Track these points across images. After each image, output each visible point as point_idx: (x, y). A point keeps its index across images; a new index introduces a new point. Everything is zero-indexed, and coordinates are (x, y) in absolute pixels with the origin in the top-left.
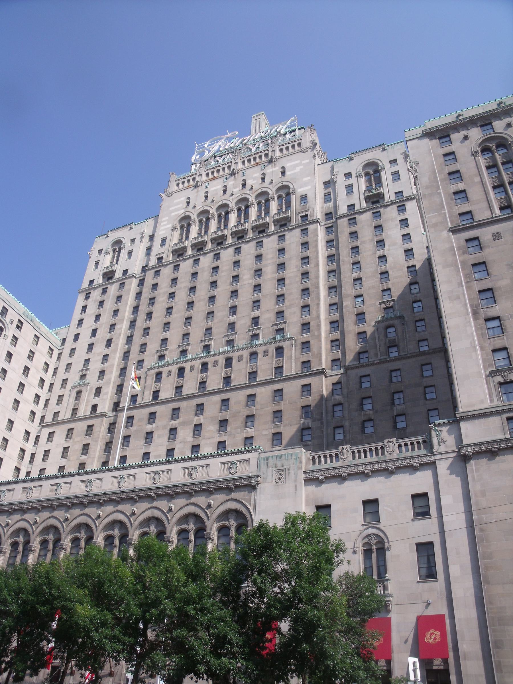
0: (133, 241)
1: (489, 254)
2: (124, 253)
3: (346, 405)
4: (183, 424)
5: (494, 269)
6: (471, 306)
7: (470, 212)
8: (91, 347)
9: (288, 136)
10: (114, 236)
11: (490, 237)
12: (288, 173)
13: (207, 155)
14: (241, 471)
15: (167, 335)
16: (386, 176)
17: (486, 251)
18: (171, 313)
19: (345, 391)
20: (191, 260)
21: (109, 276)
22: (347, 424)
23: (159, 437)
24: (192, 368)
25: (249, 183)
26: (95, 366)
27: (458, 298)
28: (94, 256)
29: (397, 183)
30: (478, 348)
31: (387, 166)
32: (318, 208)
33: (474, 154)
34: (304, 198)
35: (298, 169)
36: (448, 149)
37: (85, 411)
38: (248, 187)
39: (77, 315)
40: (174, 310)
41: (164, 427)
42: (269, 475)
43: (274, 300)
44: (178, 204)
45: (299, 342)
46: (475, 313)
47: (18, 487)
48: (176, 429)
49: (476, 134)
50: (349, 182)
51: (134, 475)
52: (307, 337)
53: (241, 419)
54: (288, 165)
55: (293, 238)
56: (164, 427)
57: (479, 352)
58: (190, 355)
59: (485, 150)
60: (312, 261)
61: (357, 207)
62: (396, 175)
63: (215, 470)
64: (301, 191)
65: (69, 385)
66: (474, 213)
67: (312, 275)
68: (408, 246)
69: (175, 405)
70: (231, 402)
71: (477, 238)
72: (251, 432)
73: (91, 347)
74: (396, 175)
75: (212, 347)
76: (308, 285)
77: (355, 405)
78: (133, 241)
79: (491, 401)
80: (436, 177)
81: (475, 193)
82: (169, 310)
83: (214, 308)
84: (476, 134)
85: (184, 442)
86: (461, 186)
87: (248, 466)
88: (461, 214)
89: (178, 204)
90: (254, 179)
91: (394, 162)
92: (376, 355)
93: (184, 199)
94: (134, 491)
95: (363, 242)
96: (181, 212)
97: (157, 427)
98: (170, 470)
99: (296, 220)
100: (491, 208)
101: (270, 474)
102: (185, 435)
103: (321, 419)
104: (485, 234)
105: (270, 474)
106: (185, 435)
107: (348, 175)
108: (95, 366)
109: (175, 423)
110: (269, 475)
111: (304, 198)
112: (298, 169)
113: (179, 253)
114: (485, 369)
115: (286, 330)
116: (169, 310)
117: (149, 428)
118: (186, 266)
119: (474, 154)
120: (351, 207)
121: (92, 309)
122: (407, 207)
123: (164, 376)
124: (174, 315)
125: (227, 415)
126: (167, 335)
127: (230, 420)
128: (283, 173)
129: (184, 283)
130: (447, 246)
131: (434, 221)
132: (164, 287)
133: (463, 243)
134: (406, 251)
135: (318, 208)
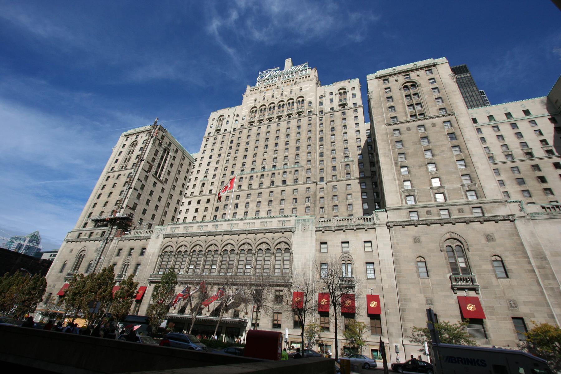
0: (229, 116)
1: (404, 137)
2: (225, 121)
3: (326, 198)
4: (252, 201)
5: (407, 144)
6: (394, 160)
7: (395, 117)
8: (209, 164)
9: (303, 72)
10: (221, 112)
11: (405, 129)
12: (303, 90)
13: (264, 78)
14: (288, 225)
15: (245, 160)
16: (349, 95)
17: (403, 136)
18: (247, 151)
19: (326, 192)
20: (257, 127)
21: (218, 131)
22: (326, 206)
23: (241, 206)
24: (257, 176)
25: (285, 93)
26: (211, 172)
27: (388, 156)
28: (210, 121)
29: (354, 99)
30: (397, 180)
31: (350, 90)
32: (316, 108)
33: (400, 89)
34: (310, 103)
35: (308, 89)
36: (387, 86)
37: (206, 192)
38: (284, 95)
39: (202, 148)
40: (249, 150)
41: (243, 202)
42: (300, 227)
43: (295, 149)
44: (251, 100)
45: (306, 169)
46: (396, 164)
47: (195, 226)
48: (249, 203)
49: (401, 79)
50: (332, 96)
51: (238, 224)
52: (309, 166)
53: (278, 201)
54: (303, 86)
55: (304, 121)
56: (243, 202)
57: (397, 181)
58: (255, 170)
59: (406, 87)
60: (313, 132)
61: (335, 109)
62: (354, 95)
63: (275, 224)
64: (309, 99)
65: (199, 180)
66: (398, 117)
67: (313, 139)
68: (357, 129)
69: (248, 192)
70: (274, 193)
71: (398, 130)
72: (283, 206)
73: (209, 164)
74: (354, 95)
75: (266, 168)
76: (310, 143)
77: (330, 198)
78: (229, 116)
79: (402, 203)
80: (380, 99)
81: (399, 108)
82: (246, 150)
83: (267, 150)
84: (401, 79)
85: (252, 209)
86: (392, 104)
87: (291, 222)
88: (392, 118)
89: (251, 100)
90: (287, 92)
91: (353, 88)
92: (340, 177)
93: (253, 98)
94: (238, 231)
95: (337, 126)
96: (252, 105)
97: (240, 202)
98: (254, 223)
99: (306, 113)
100: (406, 116)
101: (300, 227)
102: (253, 206)
103: (315, 203)
104: (403, 127)
105: (300, 227)
106: (253, 206)
107: (331, 94)
108: (211, 172)
109: (248, 200)
110: (300, 227)
111: (310, 103)
112: (308, 89)
113: (251, 123)
114: (400, 189)
115: (300, 162)
116: (246, 150)
117: (237, 201)
118: (254, 130)
119: (400, 89)
120: (332, 109)
121: (210, 146)
122: (358, 111)
123: (244, 179)
124: (249, 152)
125: (272, 198)
126: (245, 160)
127: (274, 201)
128: (301, 90)
129: (253, 138)
130: (384, 132)
131: (378, 120)
132: (244, 140)
133: (392, 131)
134: (357, 131)
135: (316, 108)
